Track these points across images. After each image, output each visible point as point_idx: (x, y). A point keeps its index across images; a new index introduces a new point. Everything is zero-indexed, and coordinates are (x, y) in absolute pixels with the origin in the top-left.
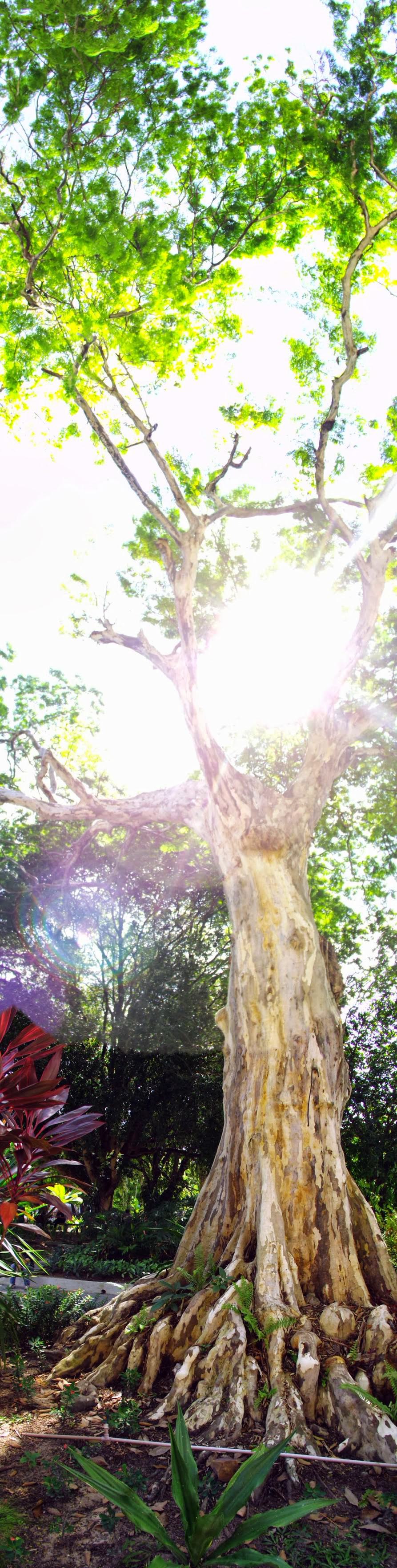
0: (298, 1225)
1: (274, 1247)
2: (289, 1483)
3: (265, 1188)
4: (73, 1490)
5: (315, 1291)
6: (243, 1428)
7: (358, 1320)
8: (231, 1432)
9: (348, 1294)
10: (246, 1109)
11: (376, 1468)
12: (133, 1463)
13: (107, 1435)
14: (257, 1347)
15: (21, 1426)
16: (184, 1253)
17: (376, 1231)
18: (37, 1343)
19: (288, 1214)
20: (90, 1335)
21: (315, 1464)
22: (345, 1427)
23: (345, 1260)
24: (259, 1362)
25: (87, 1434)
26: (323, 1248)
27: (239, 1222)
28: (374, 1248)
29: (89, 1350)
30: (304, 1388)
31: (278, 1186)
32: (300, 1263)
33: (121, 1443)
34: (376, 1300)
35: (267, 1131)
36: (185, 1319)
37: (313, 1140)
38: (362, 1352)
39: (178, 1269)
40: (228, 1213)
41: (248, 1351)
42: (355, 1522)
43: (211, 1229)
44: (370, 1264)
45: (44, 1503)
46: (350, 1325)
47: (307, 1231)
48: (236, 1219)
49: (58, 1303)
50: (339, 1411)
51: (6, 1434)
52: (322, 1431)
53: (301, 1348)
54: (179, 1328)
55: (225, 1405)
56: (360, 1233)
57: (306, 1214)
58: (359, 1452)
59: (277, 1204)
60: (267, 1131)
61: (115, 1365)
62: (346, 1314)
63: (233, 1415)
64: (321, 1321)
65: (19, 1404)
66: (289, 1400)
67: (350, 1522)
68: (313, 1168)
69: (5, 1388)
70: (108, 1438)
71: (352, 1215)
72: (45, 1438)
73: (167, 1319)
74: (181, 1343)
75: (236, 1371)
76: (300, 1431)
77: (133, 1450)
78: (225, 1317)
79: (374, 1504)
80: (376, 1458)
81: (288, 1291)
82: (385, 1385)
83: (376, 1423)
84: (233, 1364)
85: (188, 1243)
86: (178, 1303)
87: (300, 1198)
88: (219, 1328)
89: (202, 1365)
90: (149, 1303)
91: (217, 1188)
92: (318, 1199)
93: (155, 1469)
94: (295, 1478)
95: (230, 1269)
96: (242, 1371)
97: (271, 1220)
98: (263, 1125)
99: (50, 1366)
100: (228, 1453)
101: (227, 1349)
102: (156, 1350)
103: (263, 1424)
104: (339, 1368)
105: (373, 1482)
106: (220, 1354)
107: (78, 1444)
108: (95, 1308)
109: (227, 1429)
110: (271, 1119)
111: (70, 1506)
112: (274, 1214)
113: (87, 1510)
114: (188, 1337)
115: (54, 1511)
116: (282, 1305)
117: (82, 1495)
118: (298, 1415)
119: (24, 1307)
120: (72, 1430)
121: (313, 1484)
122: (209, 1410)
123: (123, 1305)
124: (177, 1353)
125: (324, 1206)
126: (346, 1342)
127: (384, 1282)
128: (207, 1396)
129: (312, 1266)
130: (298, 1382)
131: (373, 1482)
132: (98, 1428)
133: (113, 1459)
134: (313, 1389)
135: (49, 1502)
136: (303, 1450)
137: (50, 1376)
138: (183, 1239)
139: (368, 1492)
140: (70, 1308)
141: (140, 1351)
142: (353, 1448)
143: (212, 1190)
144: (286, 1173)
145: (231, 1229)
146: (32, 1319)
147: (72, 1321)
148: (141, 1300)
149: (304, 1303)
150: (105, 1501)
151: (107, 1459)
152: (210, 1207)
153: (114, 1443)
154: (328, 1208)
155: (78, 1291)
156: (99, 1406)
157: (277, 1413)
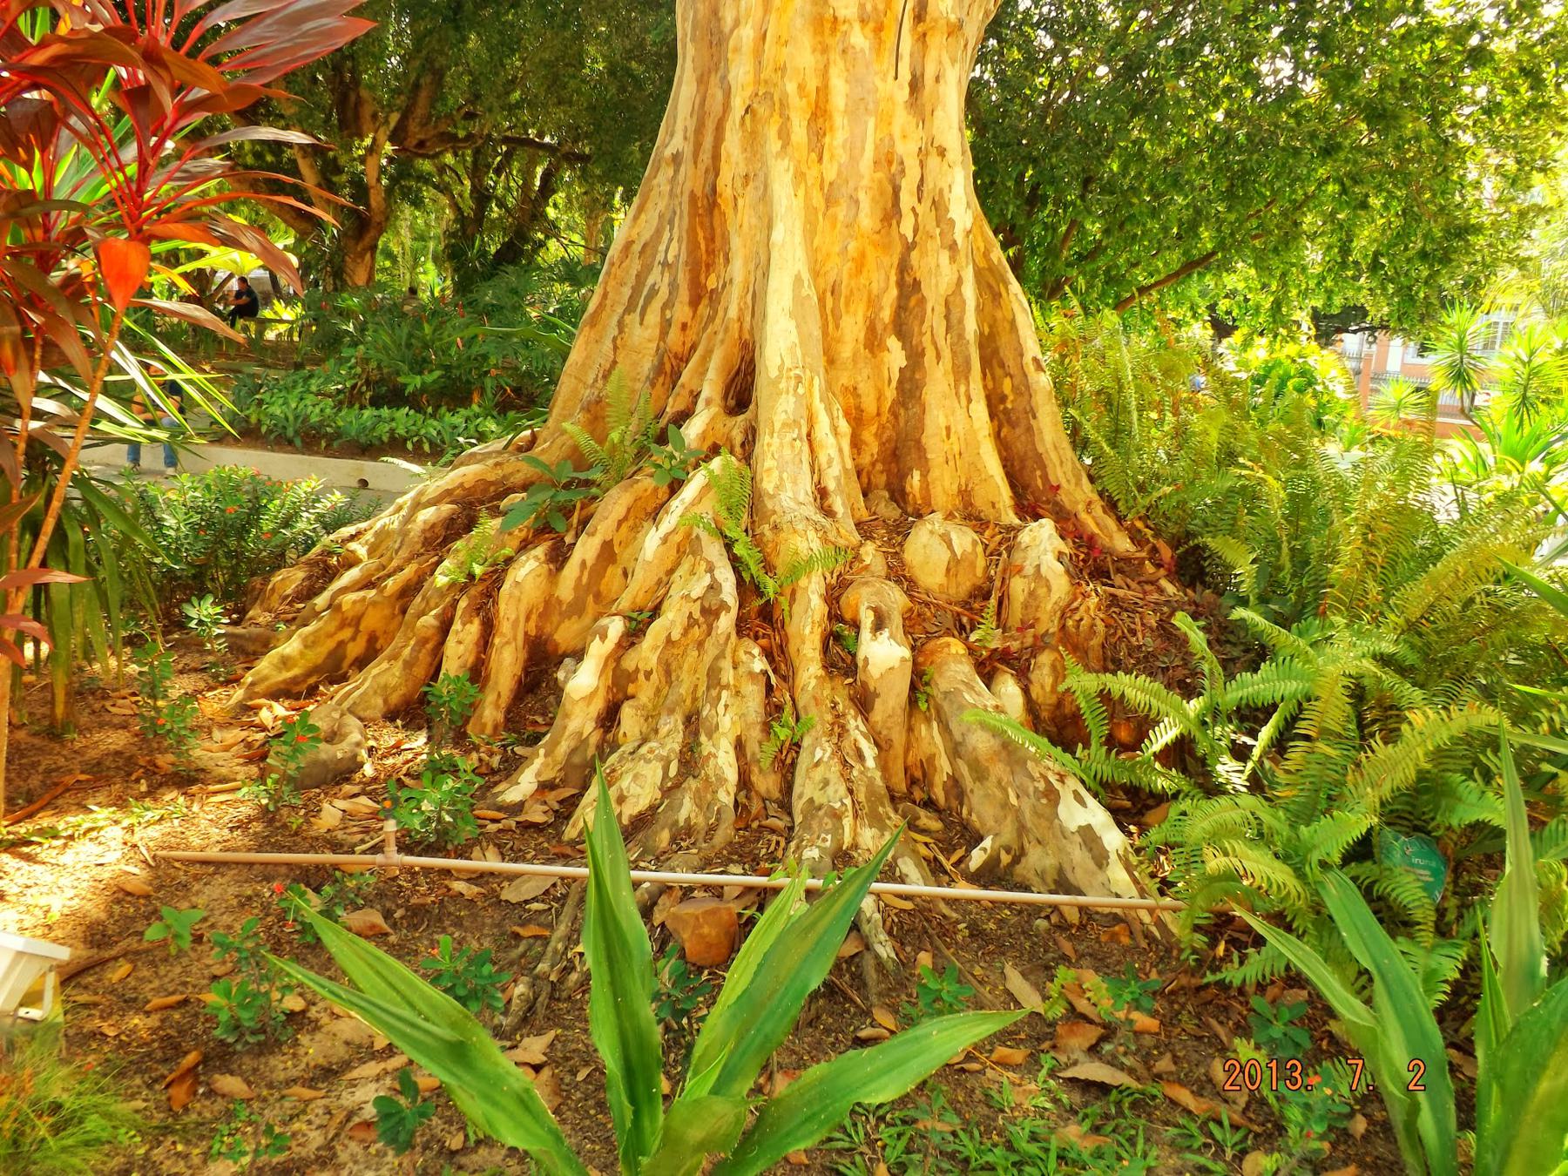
0: (852, 328)
1: (799, 379)
2: (869, 964)
3: (778, 235)
4: (291, 1016)
5: (888, 486)
6: (739, 817)
7: (992, 554)
8: (711, 830)
9: (965, 494)
10: (737, 23)
11: (1065, 910)
12: (458, 923)
13: (392, 848)
14: (762, 618)
15: (155, 832)
16: (575, 391)
17: (1032, 348)
18: (204, 610)
19: (829, 301)
20: (344, 590)
21: (923, 908)
22: (980, 808)
23: (960, 413)
24: (768, 654)
25: (336, 846)
26: (910, 386)
27: (711, 319)
28: (1024, 389)
29: (342, 626)
30: (877, 715)
31: (810, 232)
32: (857, 419)
33: (427, 871)
34: (1028, 509)
35: (791, 88)
36: (586, 549)
37: (902, 118)
38: (1001, 623)
39: (563, 427)
40: (684, 294)
41: (741, 627)
42: (1047, 1061)
43: (643, 335)
44: (1013, 425)
45: (205, 1060)
46: (973, 565)
47: (873, 342)
48: (704, 309)
49: (257, 510)
50: (964, 769)
51: (111, 857)
52: (927, 820)
53: (867, 619)
54: (571, 570)
55: (690, 761)
56: (996, 352)
57: (873, 303)
58: (1019, 869)
59: (806, 276)
60: (791, 88)
61: (408, 665)
62: (964, 539)
63: (711, 786)
64: (908, 556)
65: (151, 771)
66: (847, 745)
67: (1033, 1061)
68: (896, 191)
69: (117, 727)
70: (394, 857)
71: (979, 310)
72: (219, 865)
73: (540, 551)
74: (577, 608)
75: (713, 674)
76: (878, 822)
77: (459, 886)
78: (686, 547)
79: (1082, 1006)
80: (1063, 885)
81: (831, 485)
82: (1059, 704)
83: (1052, 795)
84: (708, 659)
85: (584, 366)
86: (567, 512)
87: (860, 264)
88: (671, 572)
89: (629, 662)
90: (495, 512)
91: (658, 233)
92: (904, 267)
93: (517, 936)
94: (885, 949)
95: (693, 430)
96: (728, 676)
97: (792, 315)
98: (781, 69)
99: (239, 669)
100: (707, 887)
101: (691, 622)
102: (515, 623)
103: (786, 807)
104: (954, 666)
105: (1067, 947)
106: (676, 636)
107: (314, 878)
108: (350, 522)
109: (699, 821)
110: (804, 57)
111: (280, 1066)
112: (798, 300)
113: (328, 1074)
114: (594, 597)
115: (230, 1083)
116: (819, 517)
117: (316, 1027)
118: (871, 780)
119: (170, 521)
120: (297, 839)
121: (925, 958)
122: (652, 774)
123: (427, 515)
124: (564, 635)
125: (917, 284)
126: (966, 605)
127: (1043, 467)
128: (644, 741)
129: (882, 427)
130: (863, 702)
131: (1067, 947)
132: (366, 831)
133: (408, 917)
134: (900, 717)
135: (220, 1057)
136: (890, 873)
137: (238, 694)
138: (574, 357)
139: (1064, 974)
140: (287, 523)
141: (474, 628)
142: (1006, 859)
143: (646, 236)
144: (830, 201)
145: (691, 335)
146: (193, 551)
147: (291, 555)
148: (465, 513)
149: (864, 515)
150: (380, 1043)
151: (387, 915)
152: (640, 278)
153: (410, 871)
154: (926, 290)
155: (308, 483)
156: (368, 770)
157: (819, 779)
